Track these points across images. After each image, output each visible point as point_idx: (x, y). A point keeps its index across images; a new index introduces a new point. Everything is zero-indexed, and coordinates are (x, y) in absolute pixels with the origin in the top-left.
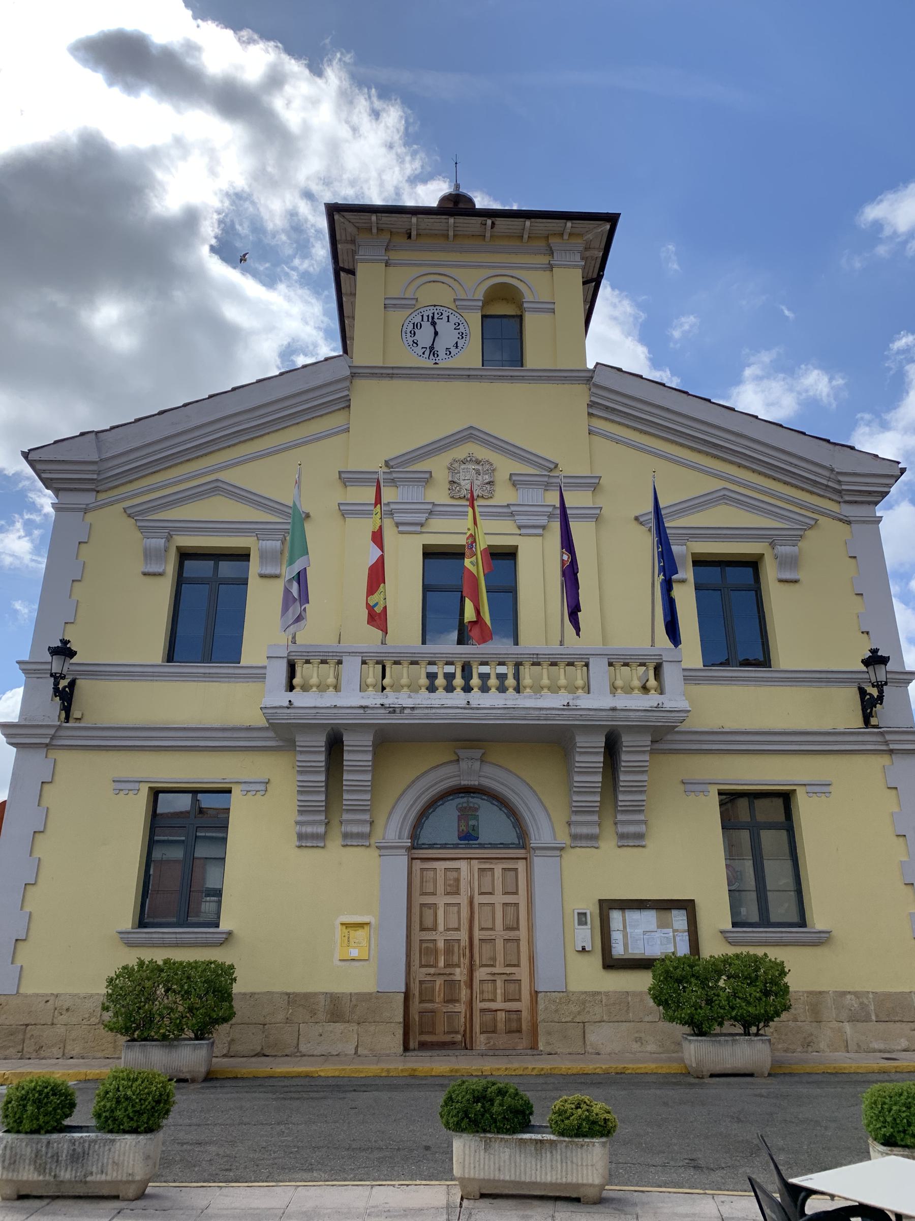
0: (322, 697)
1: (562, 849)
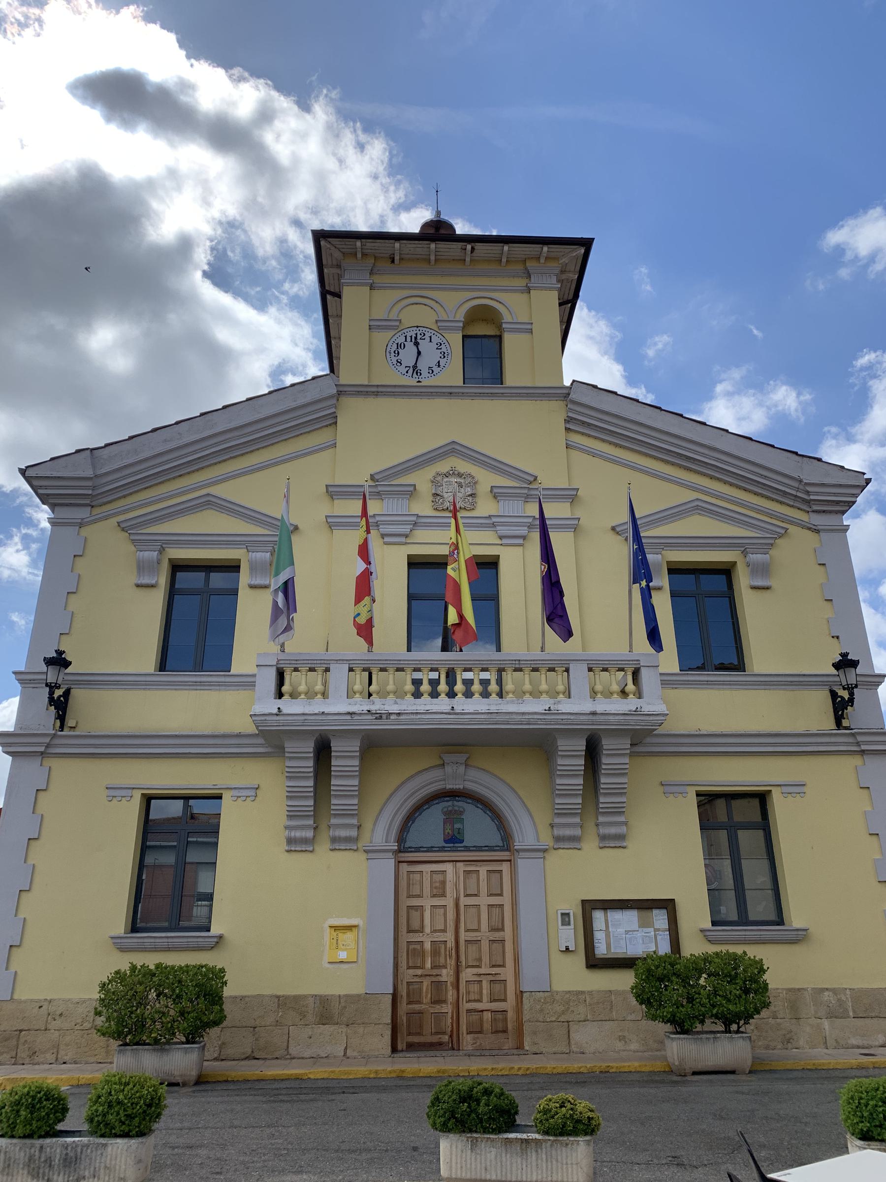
1: (545, 851)
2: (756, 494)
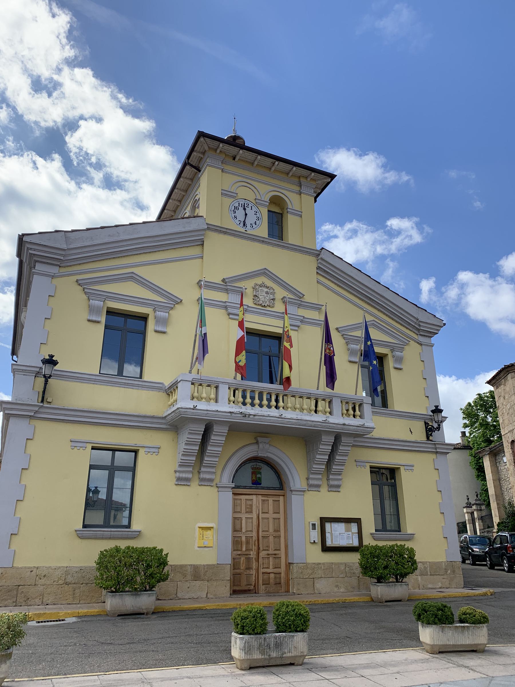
0: (209, 405)
1: (304, 491)
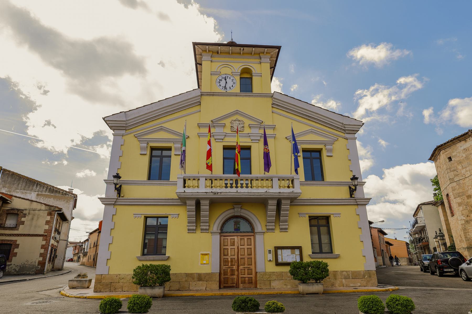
1: (264, 233)
2: (329, 128)
